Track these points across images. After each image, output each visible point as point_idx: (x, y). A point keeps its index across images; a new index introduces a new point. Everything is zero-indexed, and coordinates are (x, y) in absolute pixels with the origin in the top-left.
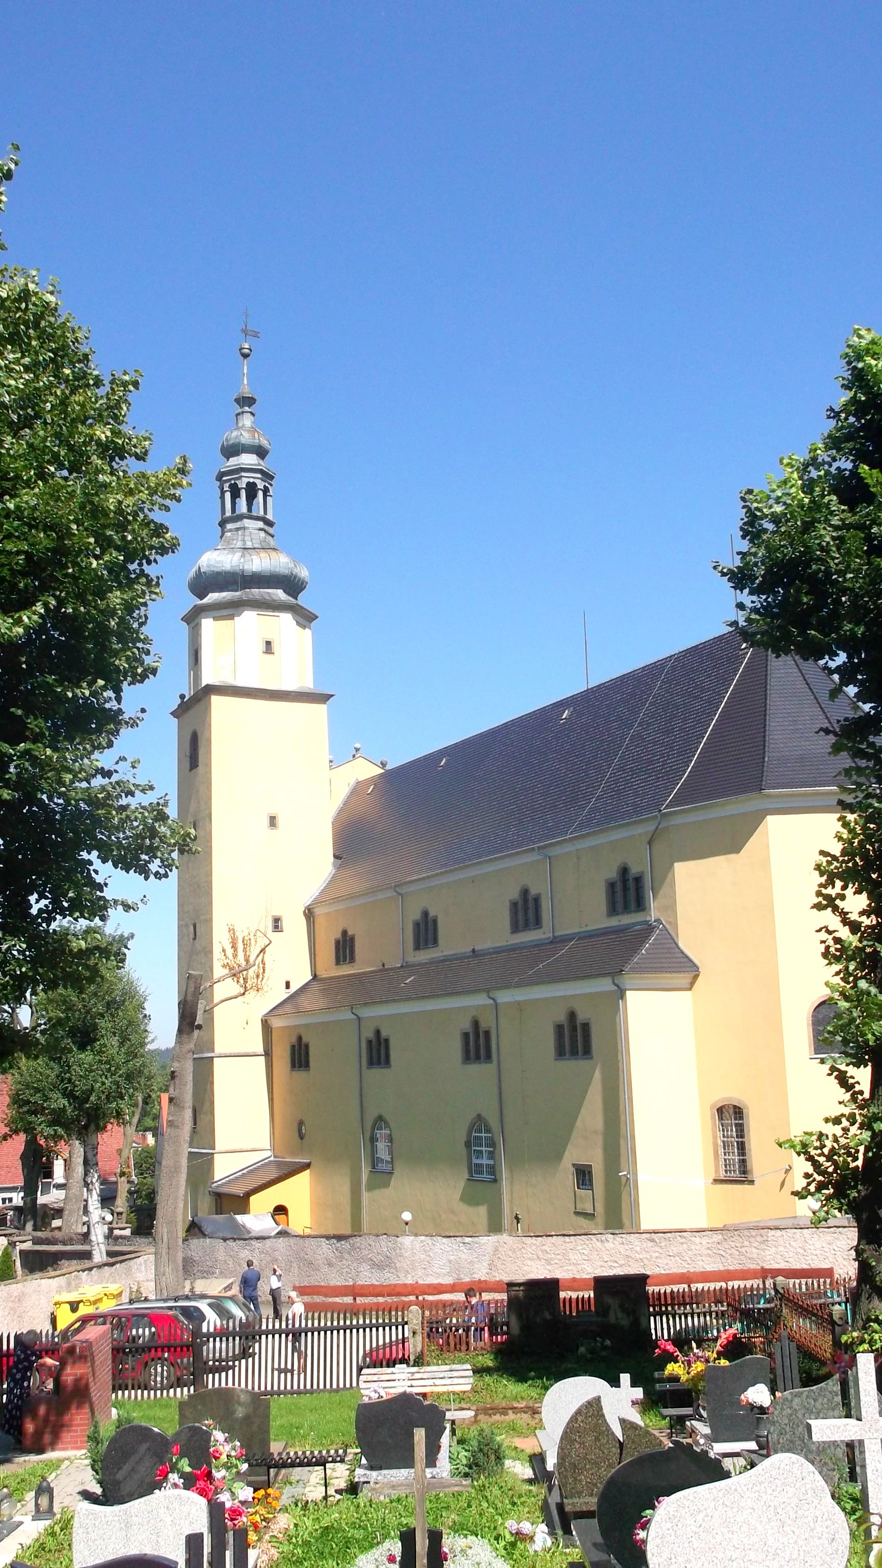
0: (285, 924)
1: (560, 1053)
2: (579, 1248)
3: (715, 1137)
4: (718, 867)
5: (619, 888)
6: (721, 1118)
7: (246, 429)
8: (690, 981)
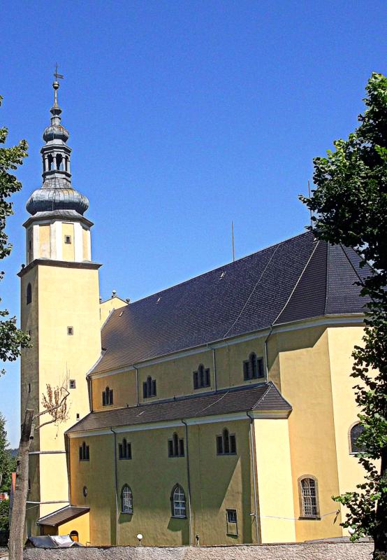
1: (220, 451)
3: (300, 495)
5: (250, 366)
6: (303, 486)
7: (56, 126)
8: (287, 414)
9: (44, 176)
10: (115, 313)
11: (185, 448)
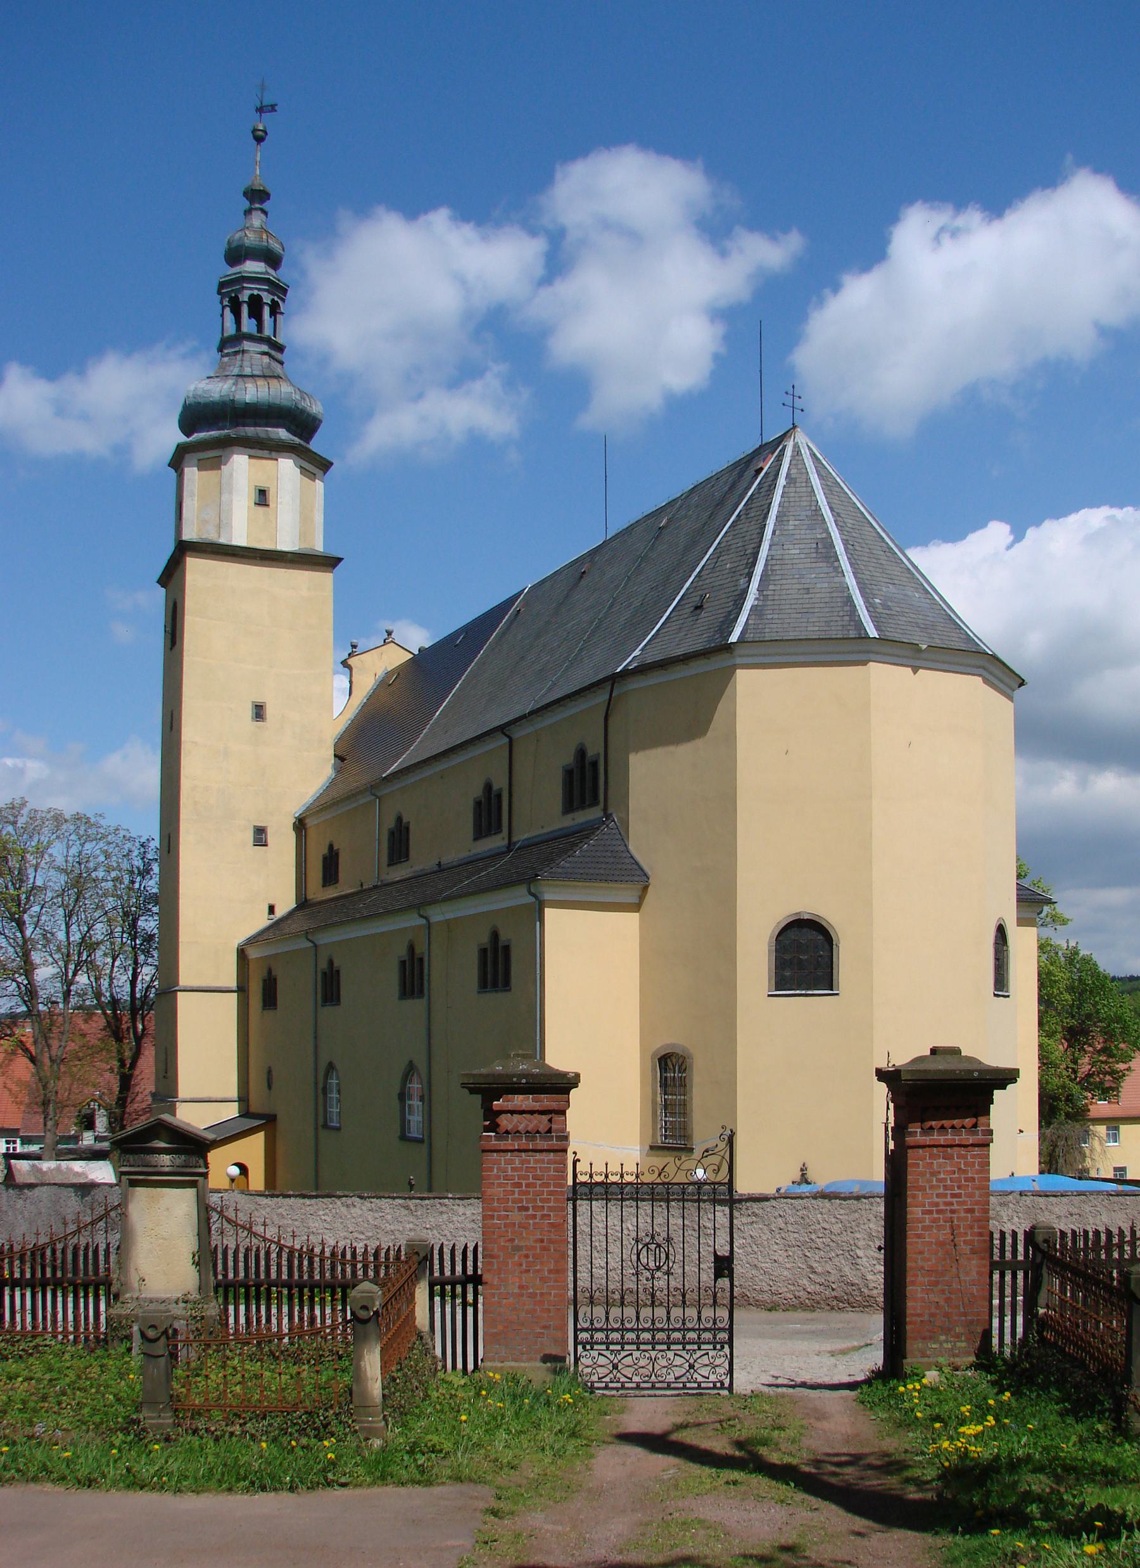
2: (321, 1213)
3: (654, 1093)
7: (254, 229)
10: (385, 684)
11: (426, 971)
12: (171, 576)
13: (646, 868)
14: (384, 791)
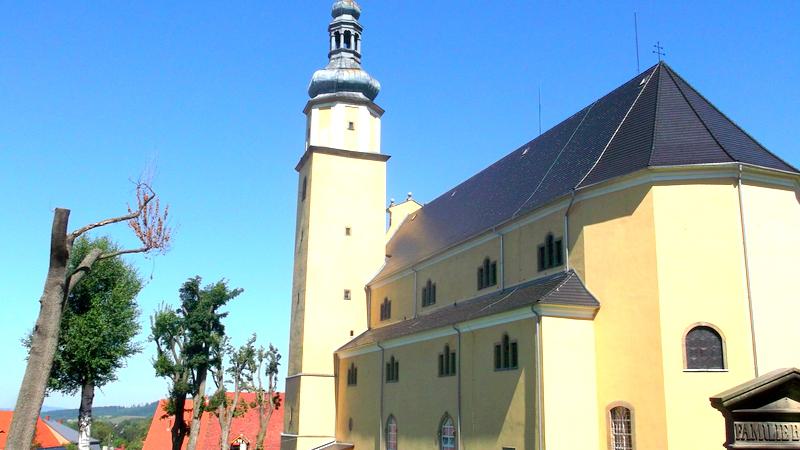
0: (352, 295)
1: (498, 366)
3: (609, 432)
4: (616, 227)
5: (546, 251)
6: (614, 417)
9: (329, 56)
12: (304, 164)
13: (597, 298)
14: (418, 268)
